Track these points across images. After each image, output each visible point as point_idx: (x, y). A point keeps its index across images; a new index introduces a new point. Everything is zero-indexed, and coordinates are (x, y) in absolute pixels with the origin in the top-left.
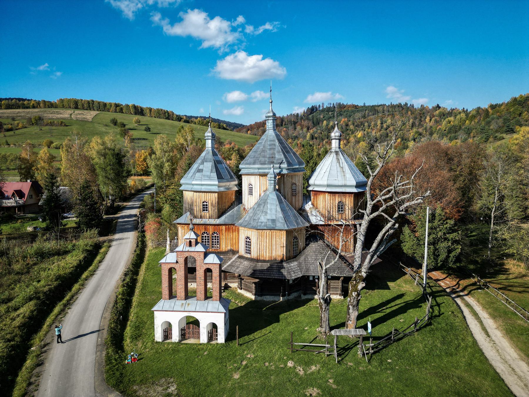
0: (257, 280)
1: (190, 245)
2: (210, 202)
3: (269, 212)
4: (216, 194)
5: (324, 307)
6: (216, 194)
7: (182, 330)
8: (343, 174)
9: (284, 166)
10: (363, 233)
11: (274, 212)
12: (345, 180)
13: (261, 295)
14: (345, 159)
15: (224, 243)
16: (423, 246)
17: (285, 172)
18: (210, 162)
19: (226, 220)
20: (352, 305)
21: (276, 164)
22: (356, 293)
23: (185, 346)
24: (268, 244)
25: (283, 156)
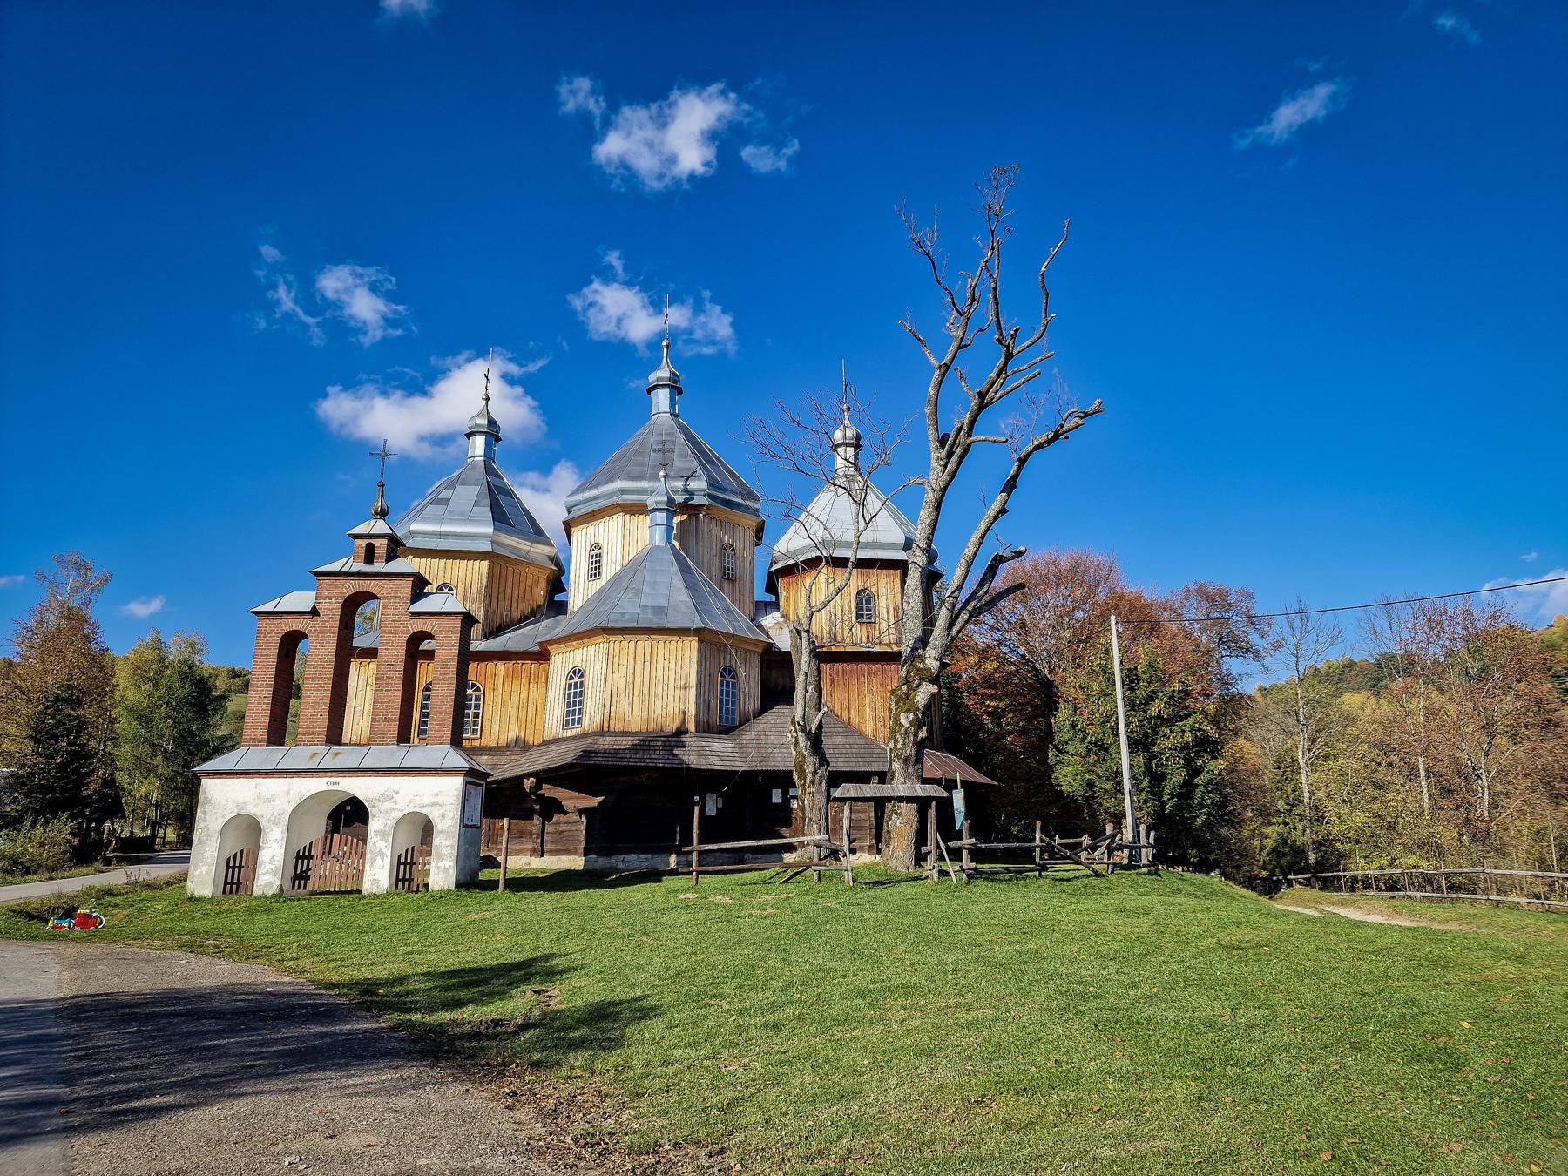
0: (595, 801)
1: (369, 557)
3: (646, 589)
4: (485, 564)
5: (809, 768)
6: (485, 564)
7: (298, 857)
13: (608, 852)
16: (1113, 750)
20: (899, 757)
21: (675, 478)
22: (911, 716)
25: (695, 463)
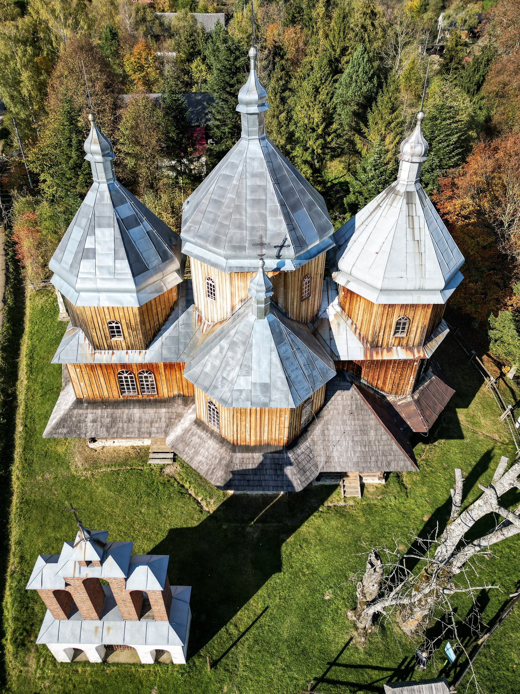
2: (123, 321)
8: (418, 262)
9: (289, 252)
10: (477, 518)
11: (265, 364)
12: (423, 276)
14: (426, 215)
15: (165, 386)
17: (289, 266)
18: (109, 226)
19: (165, 352)
23: (115, 668)
24: (253, 425)
